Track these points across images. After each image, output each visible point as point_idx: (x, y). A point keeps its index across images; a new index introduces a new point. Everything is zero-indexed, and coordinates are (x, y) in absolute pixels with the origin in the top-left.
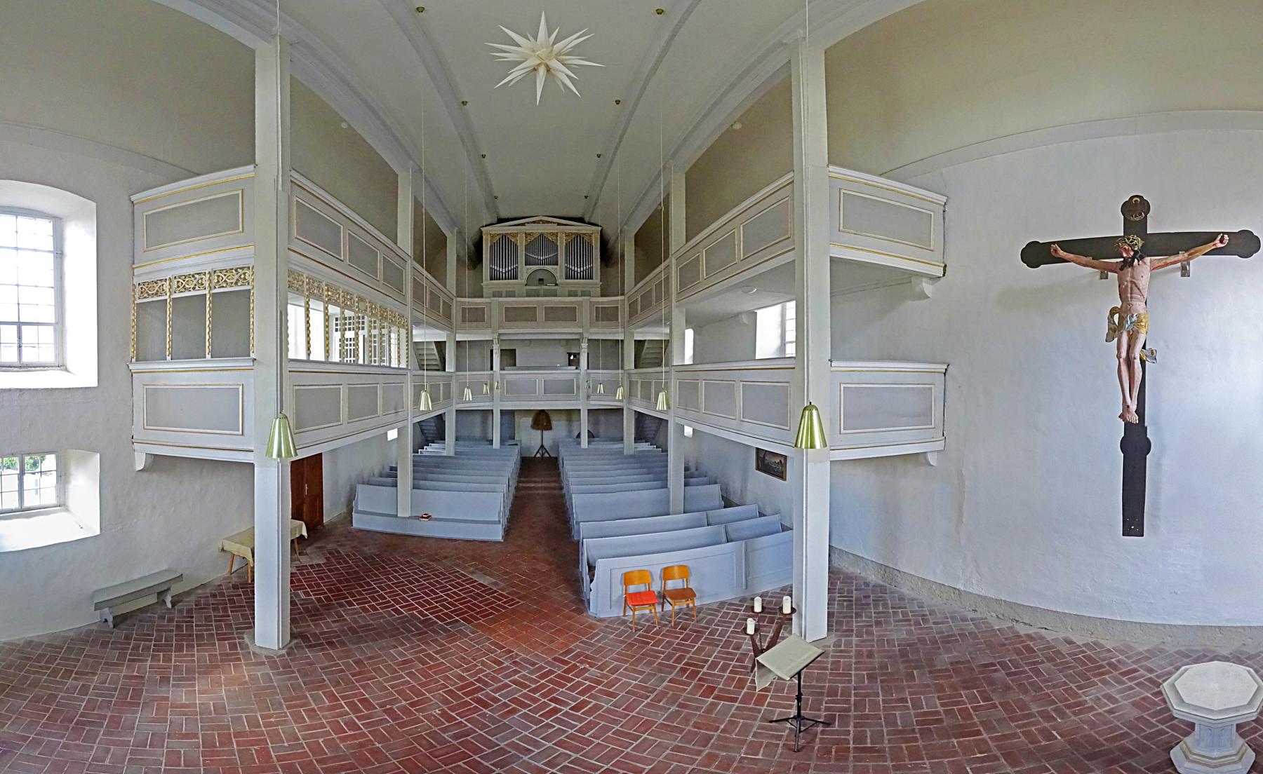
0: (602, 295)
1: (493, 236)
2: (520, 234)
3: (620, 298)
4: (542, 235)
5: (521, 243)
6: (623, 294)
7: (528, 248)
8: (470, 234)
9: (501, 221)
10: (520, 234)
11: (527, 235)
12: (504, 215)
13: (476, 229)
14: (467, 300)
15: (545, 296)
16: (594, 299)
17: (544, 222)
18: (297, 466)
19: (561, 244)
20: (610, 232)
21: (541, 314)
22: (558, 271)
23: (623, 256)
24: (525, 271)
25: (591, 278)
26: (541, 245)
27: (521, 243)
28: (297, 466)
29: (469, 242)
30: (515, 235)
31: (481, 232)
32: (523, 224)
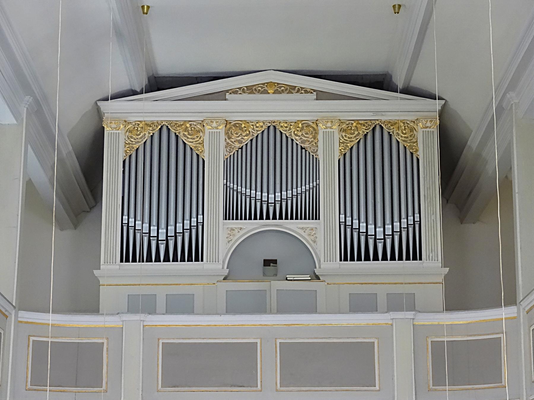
0: (452, 305)
1: (133, 129)
2: (211, 124)
3: (504, 313)
4: (272, 128)
5: (214, 151)
6: (511, 301)
7: (231, 166)
8: (69, 116)
9: (157, 84)
10: (211, 124)
11: (232, 127)
12: (167, 64)
13: (85, 105)
14: (51, 318)
15: (281, 311)
16: (425, 319)
17: (281, 89)
18: (276, 260)
19: (329, 153)
20: (470, 114)
21: (161, 303)
22: (320, 236)
23: (507, 183)
24: (223, 237)
25: (416, 256)
26: (271, 154)
27: (214, 151)
28: (276, 260)
29: (66, 149)
30: (196, 129)
31: (99, 114)
32: (220, 96)
